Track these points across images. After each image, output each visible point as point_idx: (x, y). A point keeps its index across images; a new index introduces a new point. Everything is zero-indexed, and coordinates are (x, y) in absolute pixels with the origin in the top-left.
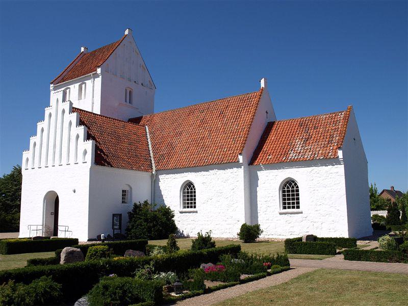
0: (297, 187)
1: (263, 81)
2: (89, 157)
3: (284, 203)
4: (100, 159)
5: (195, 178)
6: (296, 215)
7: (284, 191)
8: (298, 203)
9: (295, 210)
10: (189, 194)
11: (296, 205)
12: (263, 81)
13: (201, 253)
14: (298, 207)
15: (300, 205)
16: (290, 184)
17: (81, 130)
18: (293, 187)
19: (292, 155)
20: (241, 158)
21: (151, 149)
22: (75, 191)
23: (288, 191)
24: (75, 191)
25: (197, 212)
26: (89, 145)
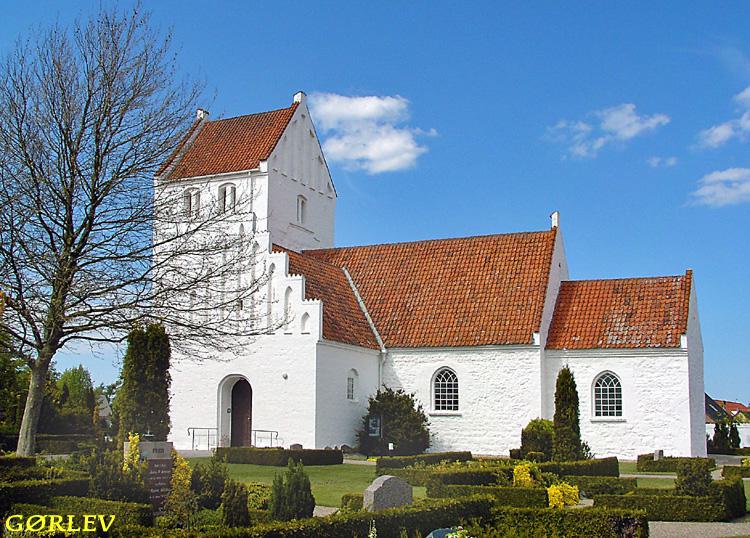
0: (619, 385)
1: (555, 216)
2: (315, 325)
3: (598, 408)
4: (333, 331)
5: (458, 362)
6: (617, 425)
7: (437, 386)
8: (619, 408)
9: (615, 418)
10: (447, 389)
11: (615, 411)
12: (555, 216)
13: (246, 533)
14: (620, 414)
15: (623, 411)
16: (608, 380)
17: (298, 283)
18: (612, 385)
19: (611, 338)
20: (537, 337)
21: (364, 309)
22: (286, 378)
23: (605, 391)
24: (286, 378)
25: (460, 416)
26: (315, 307)
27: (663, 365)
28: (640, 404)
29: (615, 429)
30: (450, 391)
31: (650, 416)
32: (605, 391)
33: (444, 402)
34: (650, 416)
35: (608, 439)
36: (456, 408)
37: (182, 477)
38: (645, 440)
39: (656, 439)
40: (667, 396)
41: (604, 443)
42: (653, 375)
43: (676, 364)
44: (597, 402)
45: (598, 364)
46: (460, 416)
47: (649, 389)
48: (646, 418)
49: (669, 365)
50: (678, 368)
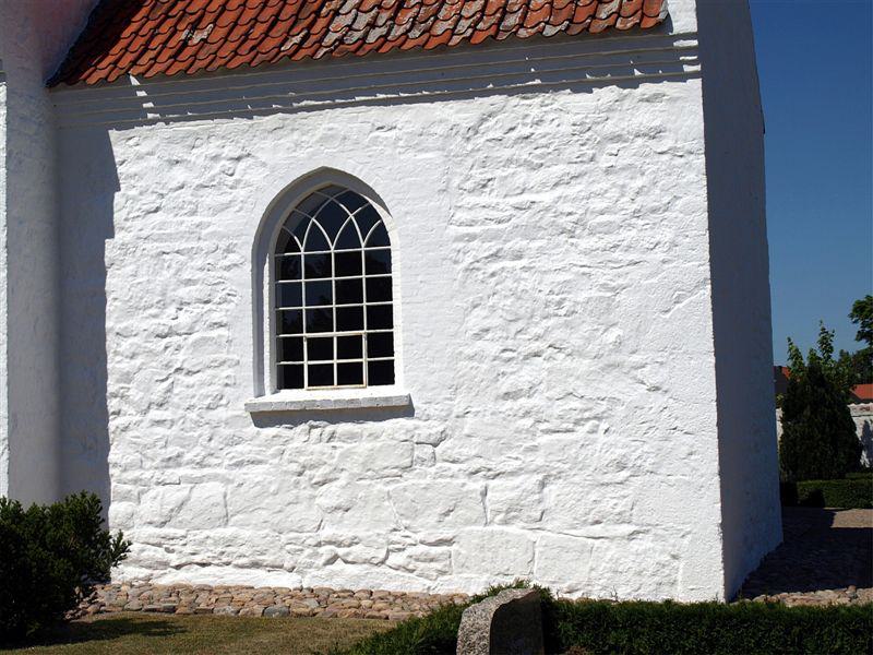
0: (382, 236)
3: (288, 349)
6: (370, 426)
8: (384, 345)
16: (332, 218)
27: (582, 128)
28: (476, 320)
29: (364, 446)
30: (350, 319)
31: (525, 375)
32: (319, 266)
33: (321, 349)
34: (525, 375)
35: (331, 495)
36: (383, 375)
37: (476, 625)
38: (502, 491)
39: (552, 490)
40: (603, 276)
41: (314, 515)
42: (537, 177)
43: (646, 117)
44: (287, 323)
45: (287, 141)
46: (406, 410)
47: (518, 243)
48: (505, 385)
49: (609, 128)
50: (655, 134)
